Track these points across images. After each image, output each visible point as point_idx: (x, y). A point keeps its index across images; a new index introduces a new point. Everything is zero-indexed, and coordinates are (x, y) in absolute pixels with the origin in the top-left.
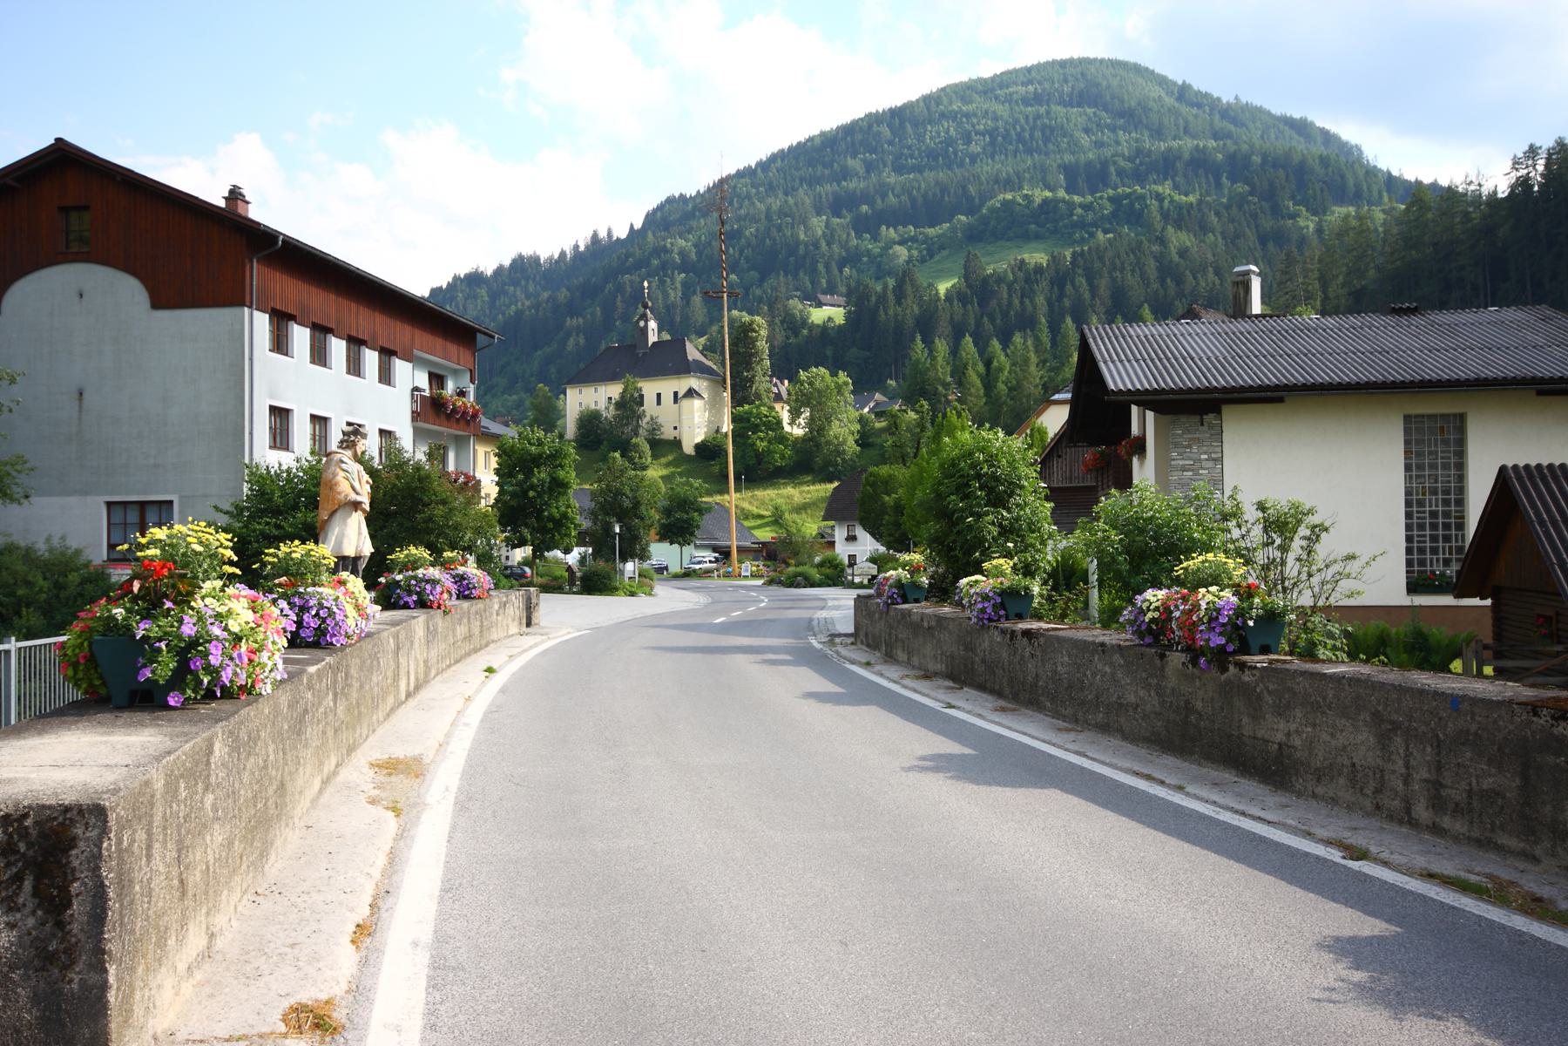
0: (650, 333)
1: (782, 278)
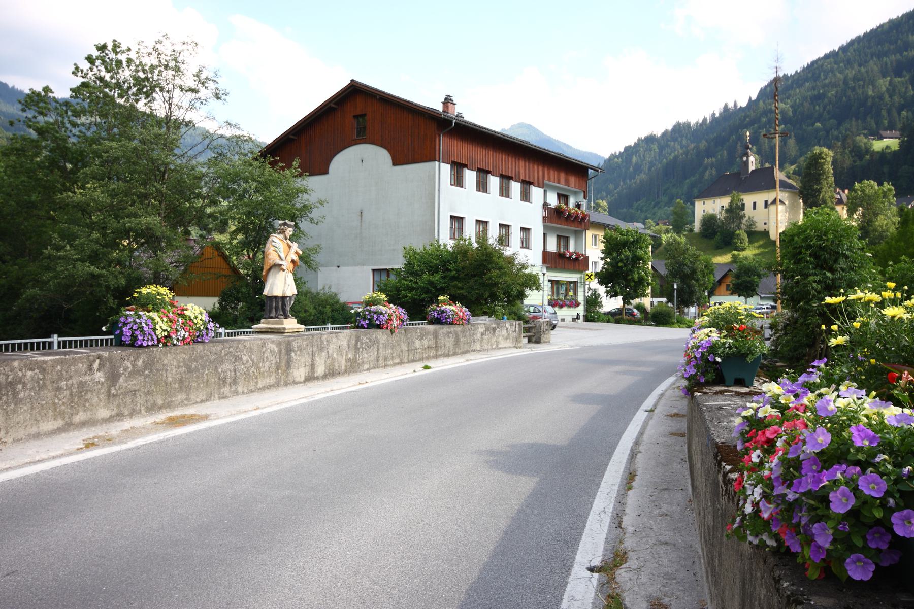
0: (750, 164)
1: (854, 123)
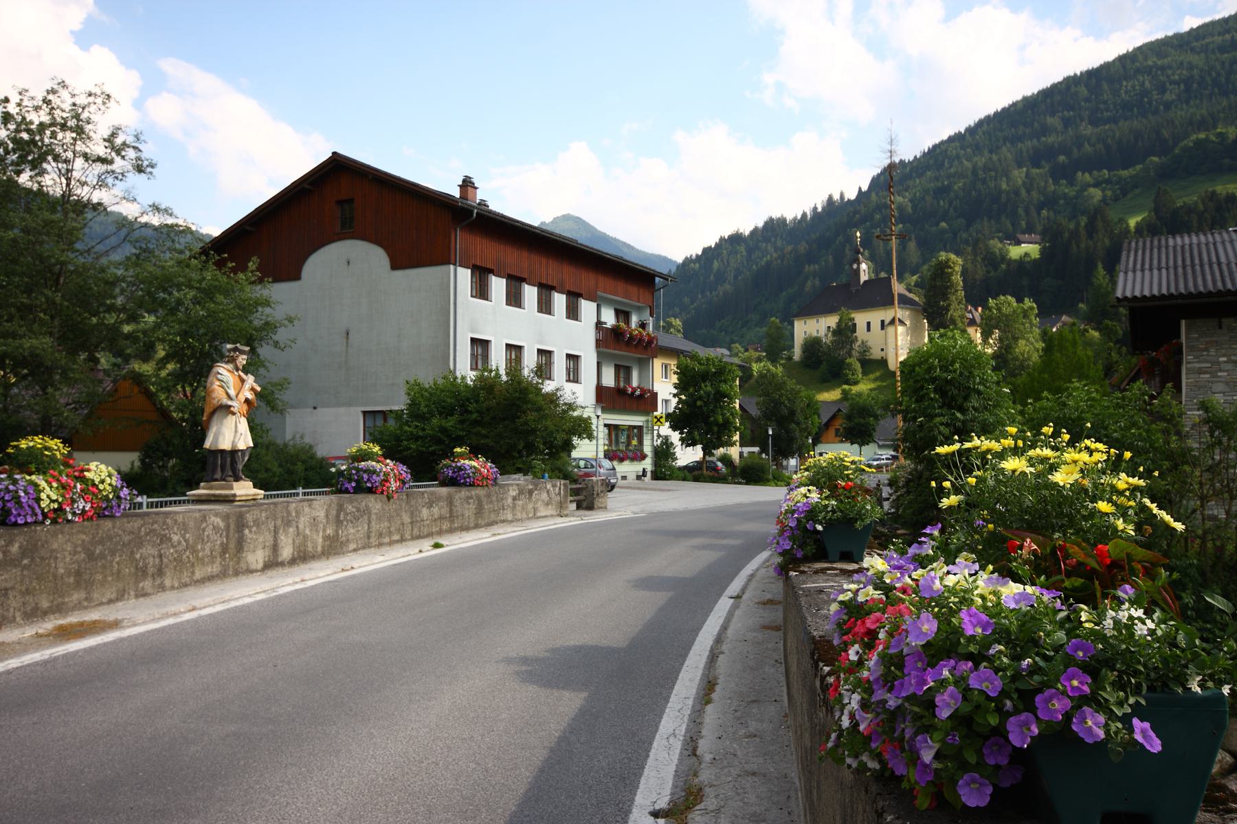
0: (862, 273)
1: (986, 223)
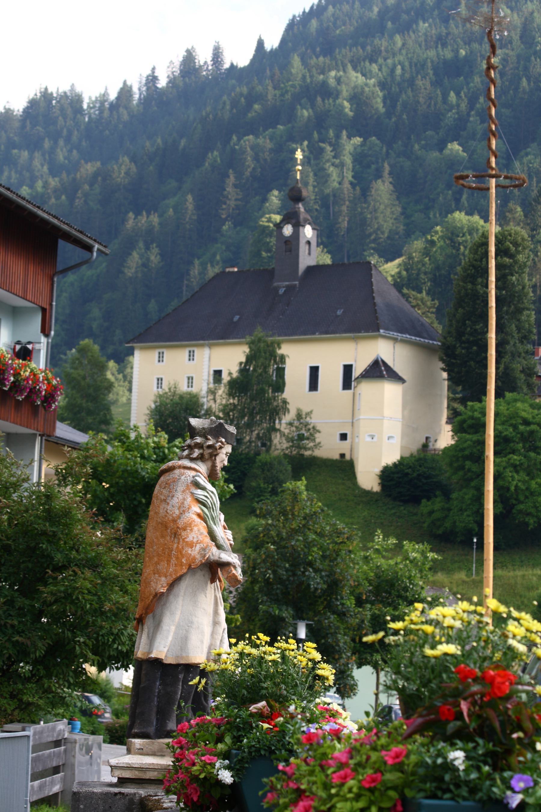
0: (303, 249)
